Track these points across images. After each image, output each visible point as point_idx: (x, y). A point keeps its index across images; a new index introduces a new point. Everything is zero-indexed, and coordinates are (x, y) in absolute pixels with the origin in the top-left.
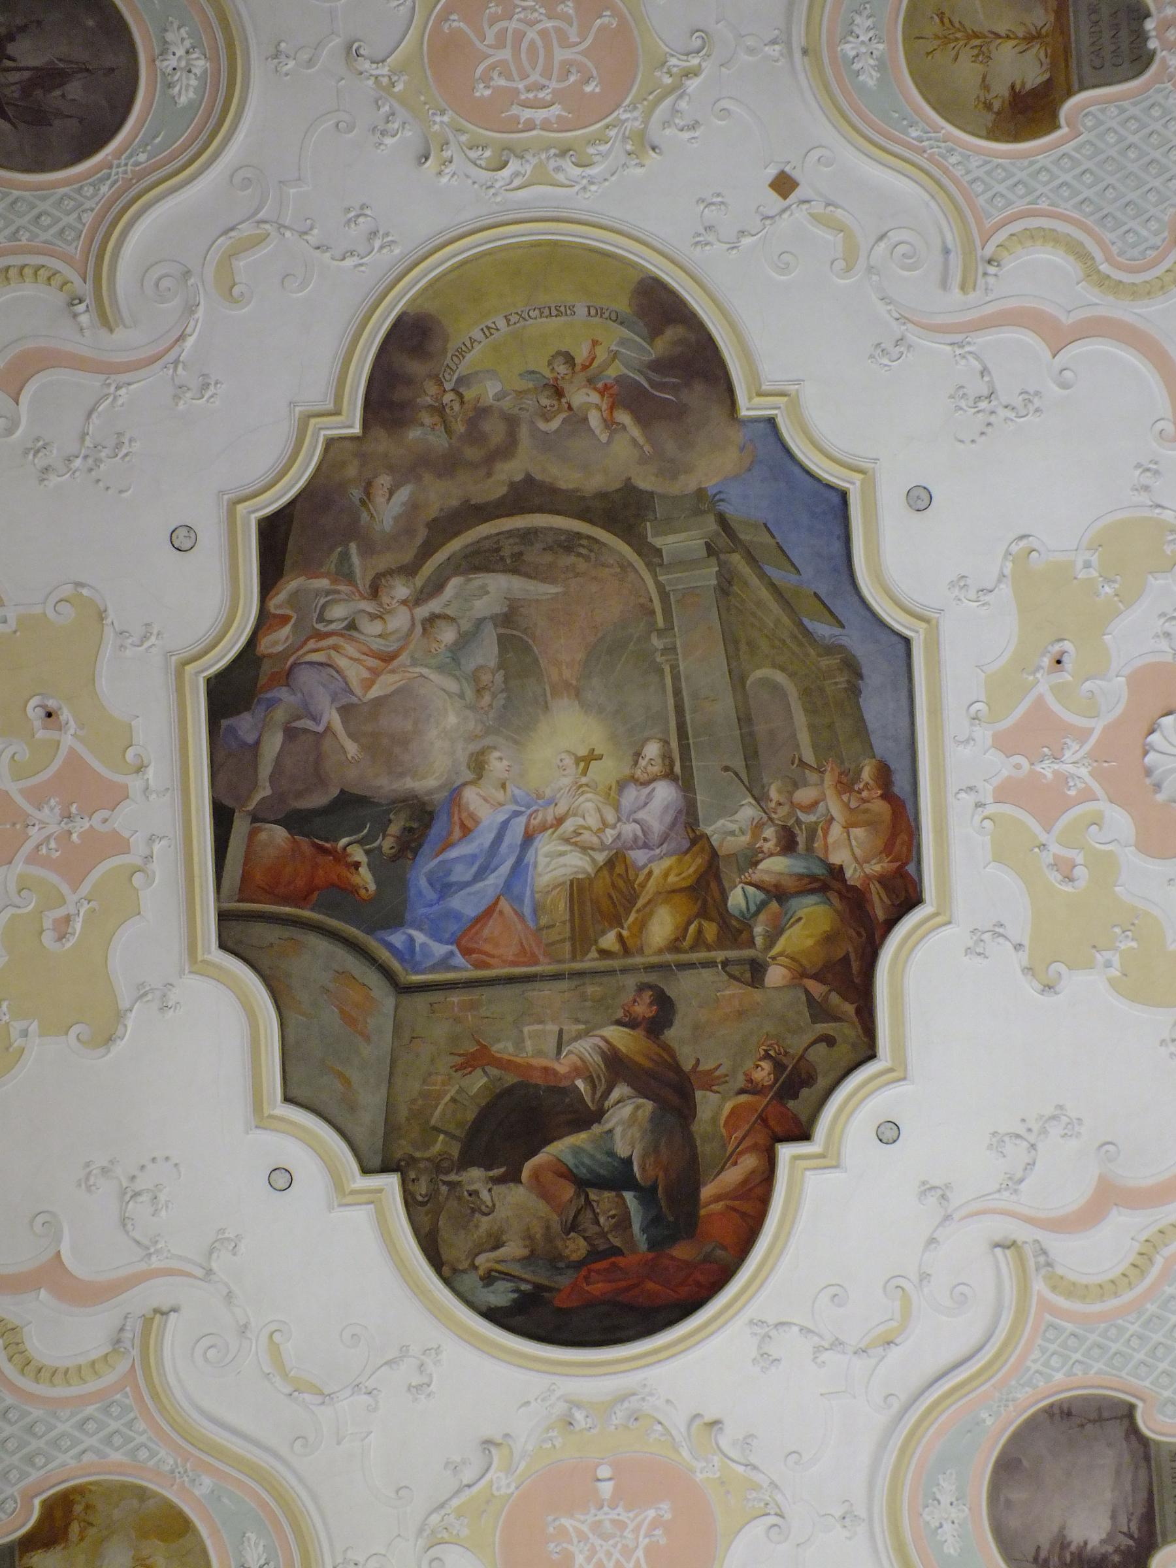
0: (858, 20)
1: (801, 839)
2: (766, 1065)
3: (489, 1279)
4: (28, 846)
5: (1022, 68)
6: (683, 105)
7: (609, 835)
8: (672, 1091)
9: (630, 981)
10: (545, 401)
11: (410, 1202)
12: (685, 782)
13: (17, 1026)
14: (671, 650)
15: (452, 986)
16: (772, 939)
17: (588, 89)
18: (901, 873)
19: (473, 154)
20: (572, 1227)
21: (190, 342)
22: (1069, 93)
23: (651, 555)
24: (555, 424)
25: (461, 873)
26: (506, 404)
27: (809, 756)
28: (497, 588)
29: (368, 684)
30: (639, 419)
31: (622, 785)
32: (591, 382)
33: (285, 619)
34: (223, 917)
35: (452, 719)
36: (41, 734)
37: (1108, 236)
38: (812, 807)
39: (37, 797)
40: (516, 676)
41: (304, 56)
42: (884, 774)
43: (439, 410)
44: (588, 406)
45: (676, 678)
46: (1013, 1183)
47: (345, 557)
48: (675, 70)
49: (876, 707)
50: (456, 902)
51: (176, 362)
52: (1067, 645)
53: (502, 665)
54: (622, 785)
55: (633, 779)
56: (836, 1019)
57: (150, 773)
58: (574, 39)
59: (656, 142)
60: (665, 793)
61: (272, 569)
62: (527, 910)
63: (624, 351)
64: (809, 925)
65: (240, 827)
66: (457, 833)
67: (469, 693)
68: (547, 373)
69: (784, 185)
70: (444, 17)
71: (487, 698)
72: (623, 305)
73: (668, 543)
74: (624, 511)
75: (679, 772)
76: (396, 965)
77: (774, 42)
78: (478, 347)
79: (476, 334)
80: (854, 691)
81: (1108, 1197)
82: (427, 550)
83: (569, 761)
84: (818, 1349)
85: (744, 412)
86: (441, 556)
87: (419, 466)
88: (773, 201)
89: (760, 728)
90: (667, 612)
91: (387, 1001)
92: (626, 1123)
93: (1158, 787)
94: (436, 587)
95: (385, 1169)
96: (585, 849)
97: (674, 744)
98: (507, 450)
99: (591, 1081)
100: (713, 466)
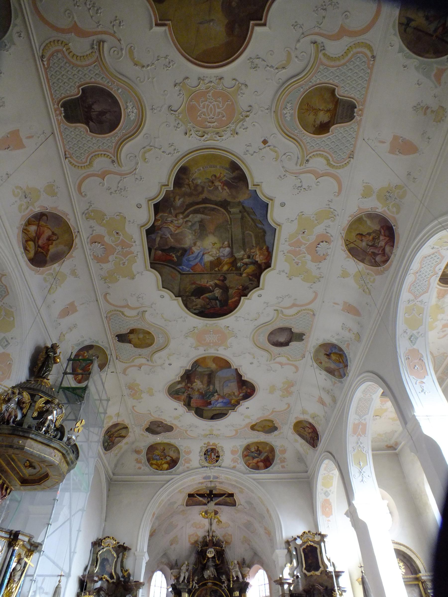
0: (288, 105)
1: (251, 257)
2: (241, 287)
3: (195, 309)
4: (116, 252)
5: (323, 117)
6: (244, 123)
7: (217, 255)
8: (225, 289)
9: (220, 275)
10: (210, 184)
11: (183, 301)
12: (232, 248)
13: (118, 276)
14: (231, 228)
15: (189, 274)
16: (244, 270)
17: (223, 119)
18: (268, 262)
19: (196, 133)
20: (208, 304)
21: (137, 170)
22: (334, 124)
23: (229, 212)
24: (212, 188)
25: (191, 259)
26: (202, 184)
27: (255, 245)
28: (199, 217)
29: (175, 231)
30: (228, 188)
31: (220, 248)
32: (219, 181)
33: (160, 220)
34: (151, 263)
35: (190, 237)
36: (116, 236)
37: (334, 156)
38: (254, 252)
39: (117, 245)
40: (202, 231)
41: (159, 109)
42: (268, 248)
43: (189, 185)
44: (219, 185)
45: (232, 232)
46: (279, 303)
47: (171, 210)
48: (243, 115)
49: (268, 238)
50: (191, 263)
51: (135, 174)
52: (306, 230)
53: (199, 229)
54: (220, 248)
55: (222, 247)
56: (253, 281)
57: (137, 243)
58: (221, 107)
59: (237, 131)
60: (228, 249)
61: (156, 213)
62: (203, 265)
63: (226, 175)
64: (251, 269)
65: (153, 251)
66: (191, 253)
67: (194, 233)
68: (211, 179)
69: (265, 142)
70: (191, 101)
71: (196, 234)
72: (227, 166)
73: (232, 210)
74: (225, 204)
75: (231, 246)
76: (180, 271)
77: (267, 109)
78: (197, 173)
79: (196, 170)
80: (264, 236)
81: (294, 305)
82: (186, 210)
83: (211, 244)
84: (245, 320)
85: (250, 189)
86: (188, 211)
87: (184, 195)
88: (262, 146)
89: (246, 240)
90: (231, 222)
91: (179, 276)
92: (217, 292)
93: (317, 253)
94: (188, 216)
95: (179, 296)
96: (213, 257)
97: (230, 242)
98: (202, 192)
99: (212, 287)
100: (243, 197)
